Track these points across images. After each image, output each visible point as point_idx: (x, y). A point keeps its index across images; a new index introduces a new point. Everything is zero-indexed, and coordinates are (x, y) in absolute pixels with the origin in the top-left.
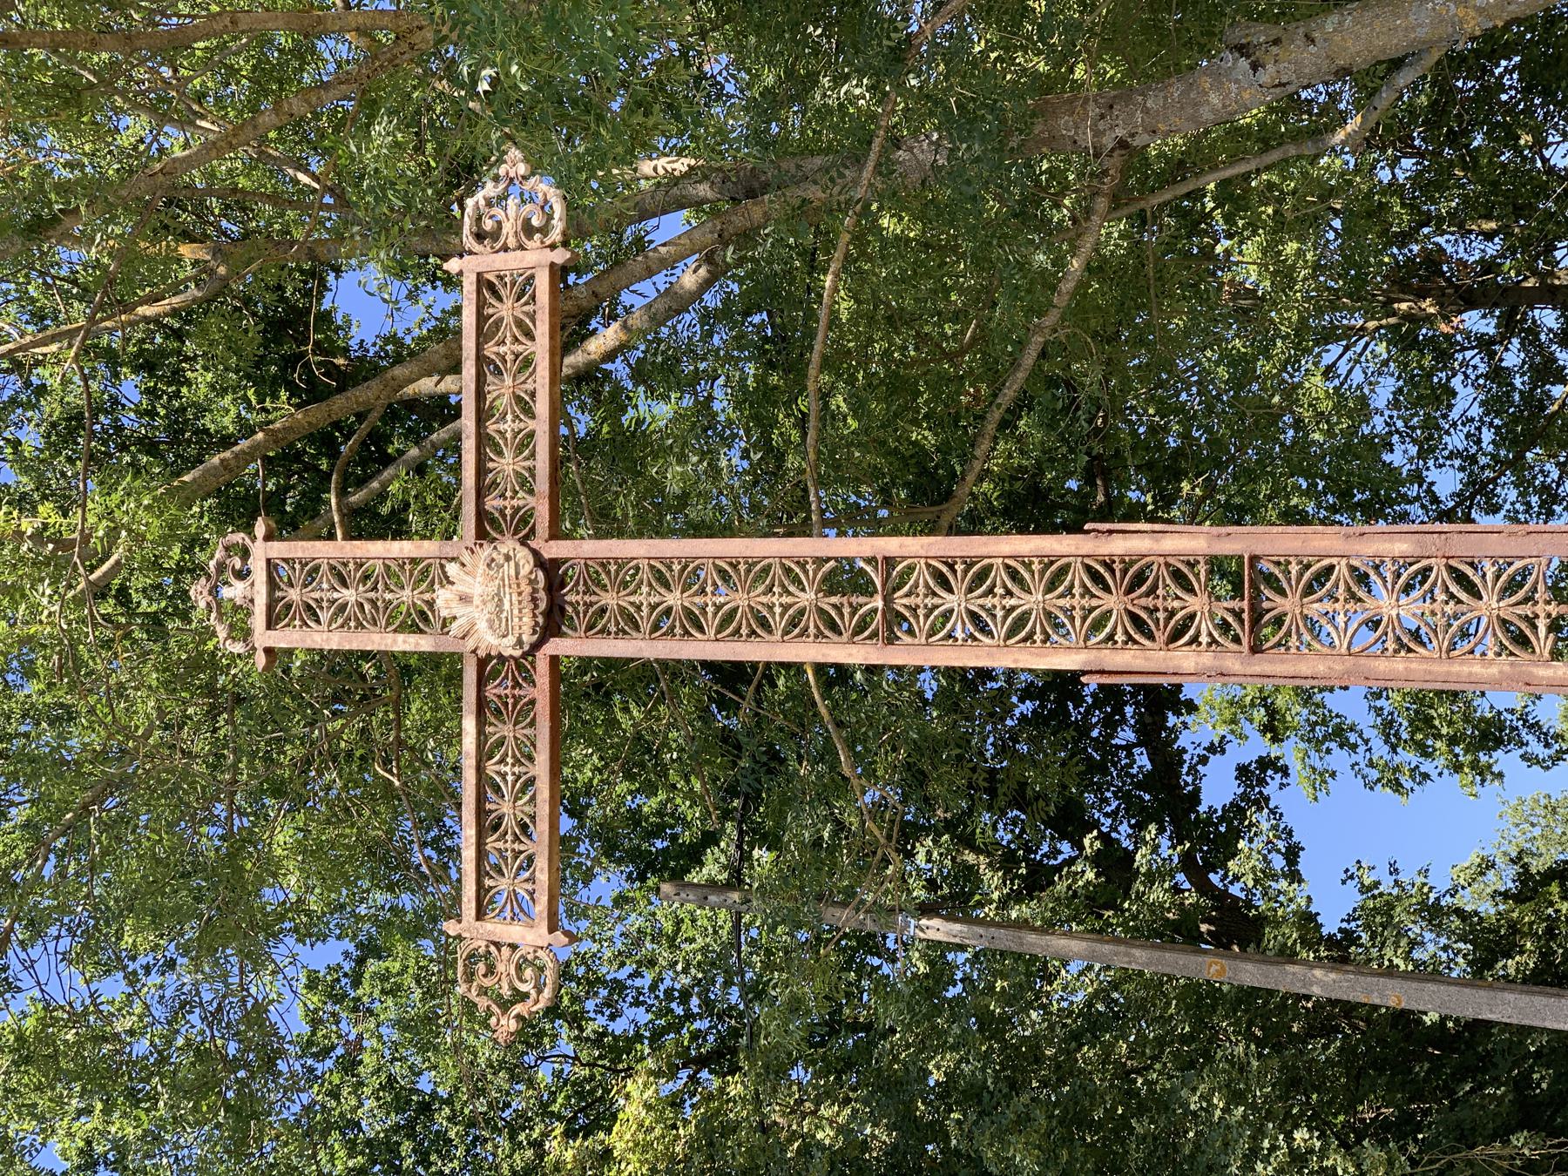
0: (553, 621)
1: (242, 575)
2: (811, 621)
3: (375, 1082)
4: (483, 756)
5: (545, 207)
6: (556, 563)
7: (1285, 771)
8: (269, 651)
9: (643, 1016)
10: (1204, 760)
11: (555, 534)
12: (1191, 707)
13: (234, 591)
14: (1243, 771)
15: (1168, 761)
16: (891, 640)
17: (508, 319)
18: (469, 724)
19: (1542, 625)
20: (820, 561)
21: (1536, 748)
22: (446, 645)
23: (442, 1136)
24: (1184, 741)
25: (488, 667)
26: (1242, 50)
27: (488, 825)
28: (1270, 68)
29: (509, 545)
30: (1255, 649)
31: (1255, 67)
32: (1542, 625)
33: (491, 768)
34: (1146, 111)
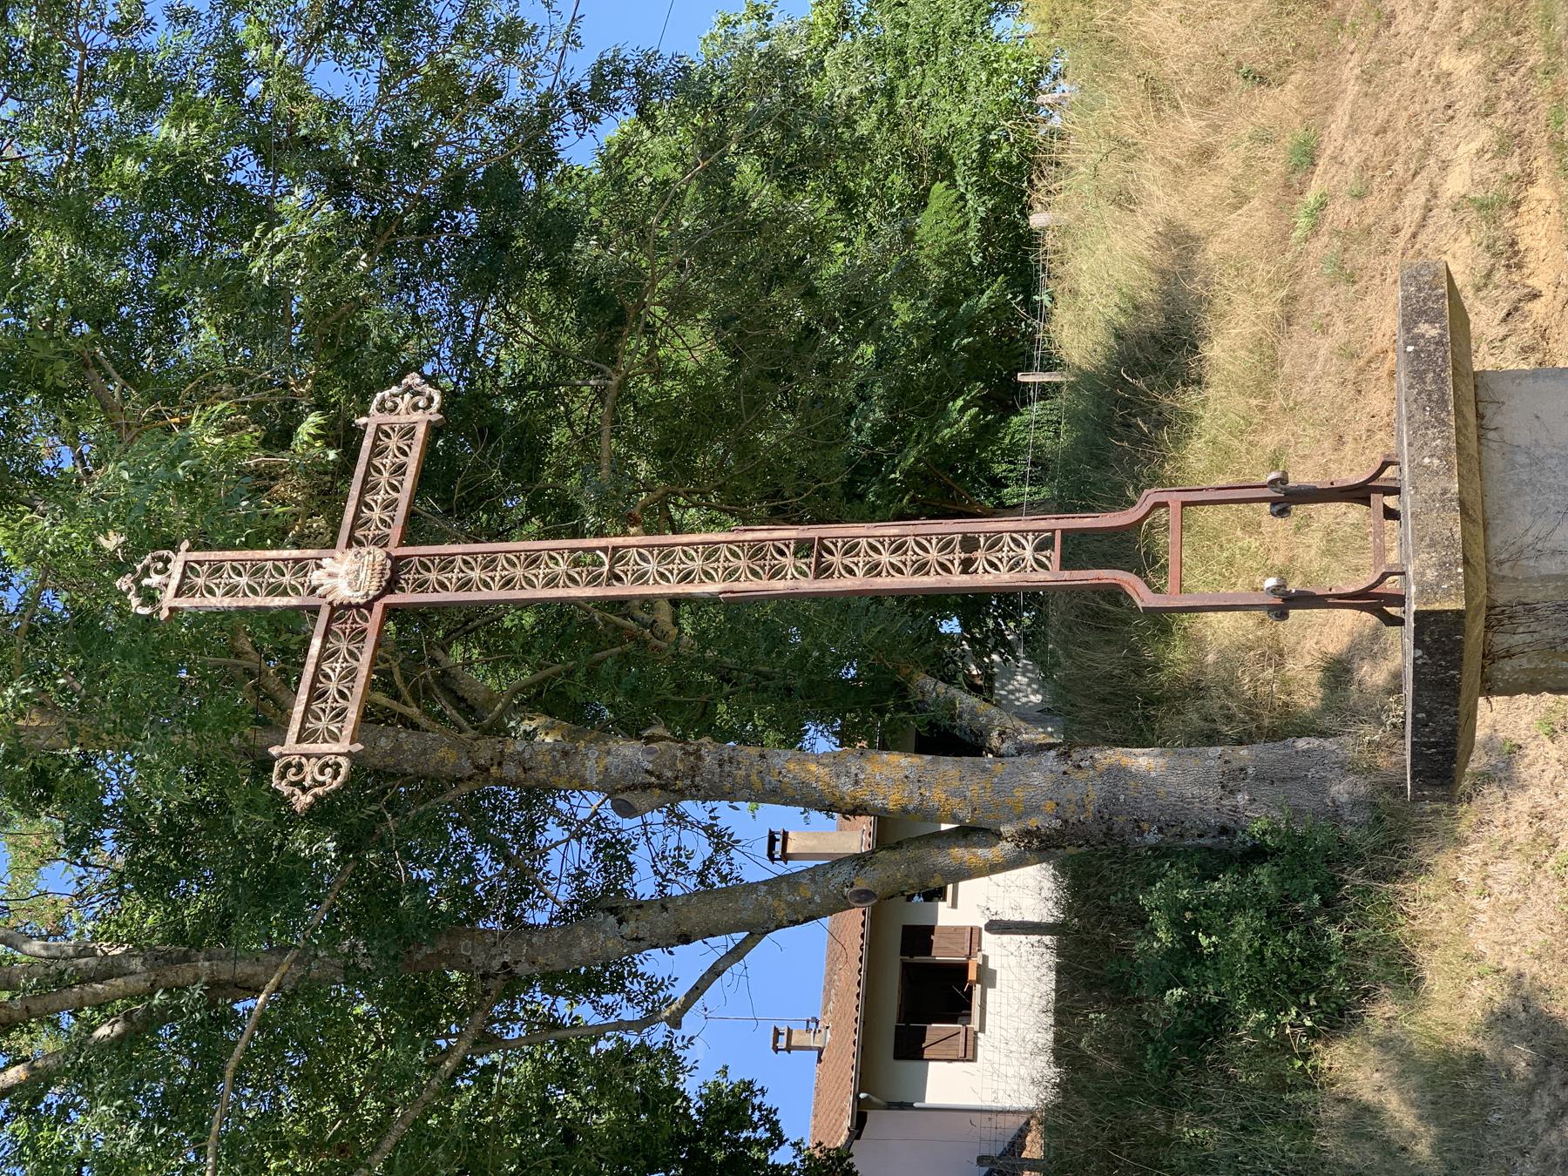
4: (321, 658)
13: (154, 580)
19: (956, 562)
22: (313, 601)
25: (340, 611)
27: (316, 694)
28: (632, 924)
31: (620, 922)
32: (956, 562)
34: (531, 945)
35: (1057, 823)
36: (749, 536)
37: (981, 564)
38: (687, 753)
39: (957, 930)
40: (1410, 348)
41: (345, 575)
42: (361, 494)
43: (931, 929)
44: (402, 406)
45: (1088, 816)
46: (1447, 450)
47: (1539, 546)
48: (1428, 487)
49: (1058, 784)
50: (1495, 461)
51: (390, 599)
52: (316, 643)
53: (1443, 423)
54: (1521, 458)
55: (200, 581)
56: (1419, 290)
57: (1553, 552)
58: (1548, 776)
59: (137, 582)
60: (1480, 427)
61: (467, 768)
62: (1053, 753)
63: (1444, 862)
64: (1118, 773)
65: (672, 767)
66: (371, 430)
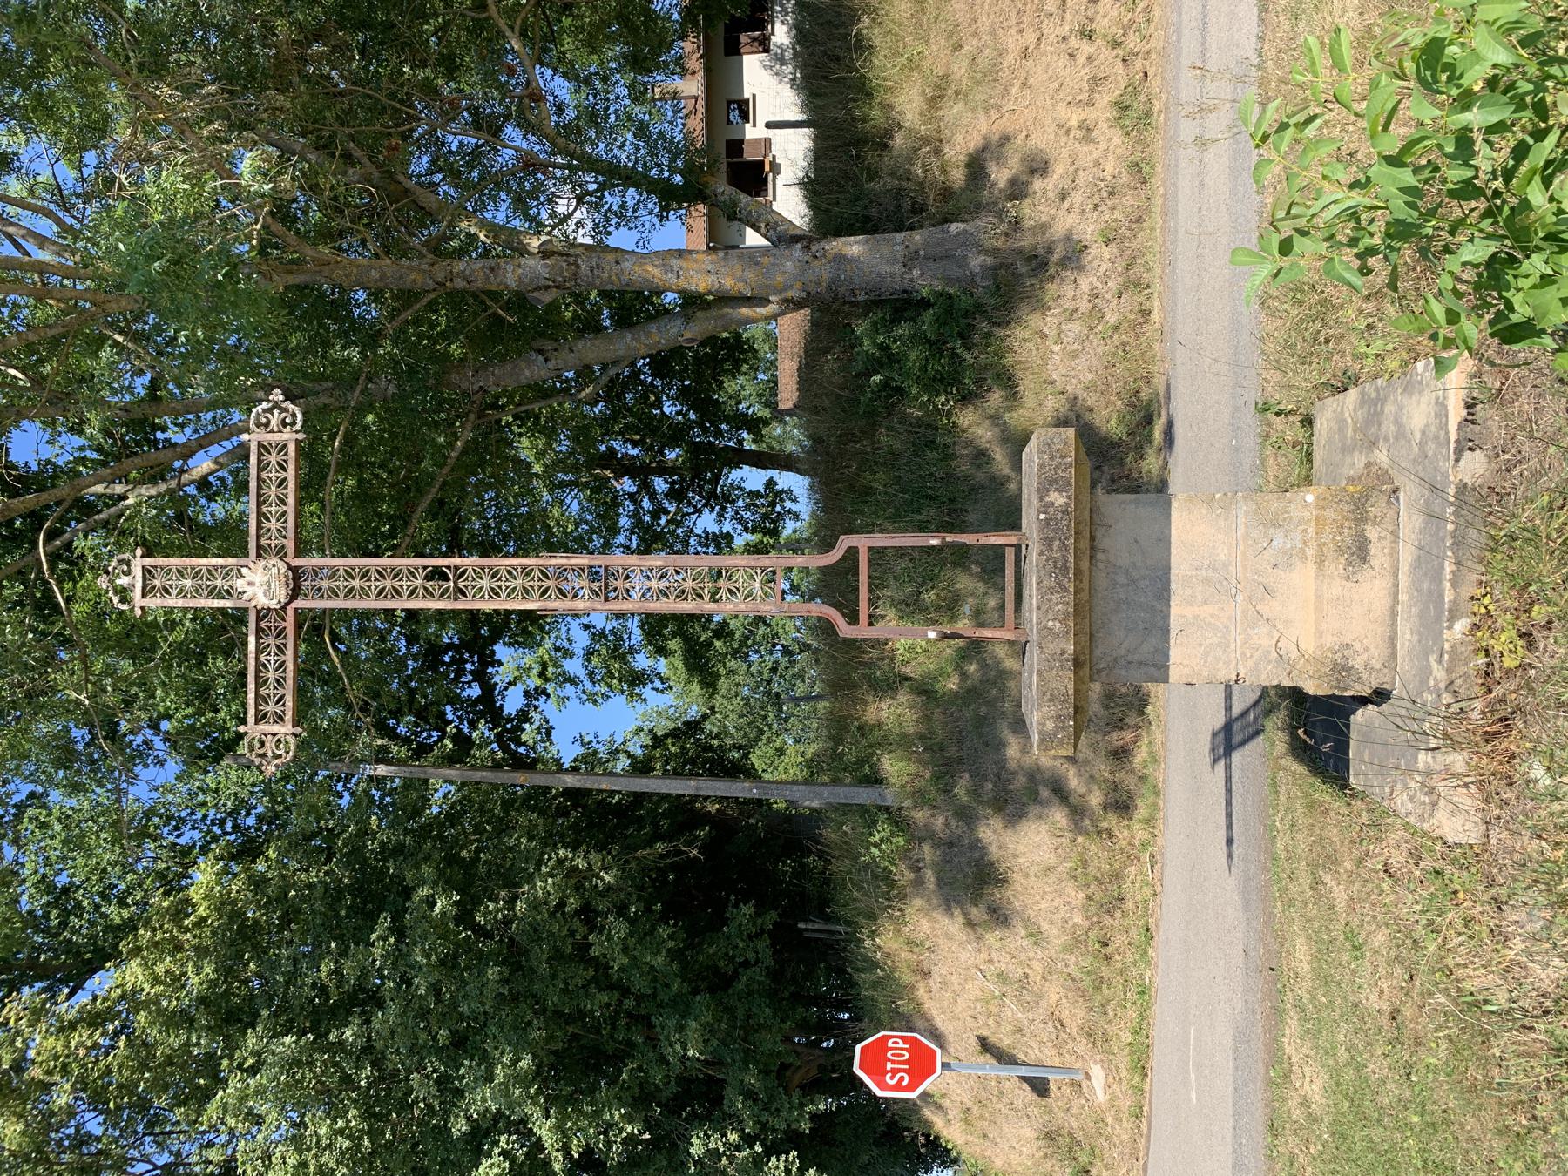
0: (294, 595)
1: (127, 573)
2: (420, 592)
3: (34, 879)
4: (258, 653)
5: (294, 415)
6: (297, 568)
7: (548, 696)
8: (142, 608)
9: (196, 835)
10: (506, 689)
11: (297, 555)
12: (500, 663)
13: (124, 581)
14: (527, 693)
15: (488, 688)
16: (456, 599)
17: (273, 462)
18: (252, 640)
20: (425, 568)
21: (658, 684)
23: (79, 905)
24: (497, 679)
25: (262, 614)
26: (540, 352)
27: (260, 682)
29: (275, 560)
30: (607, 600)
31: (546, 360)
33: (262, 657)
35: (803, 294)
36: (553, 562)
37: (723, 593)
38: (569, 264)
39: (757, 141)
40: (1042, 516)
41: (259, 584)
42: (258, 507)
43: (742, 141)
44: (274, 423)
45: (823, 289)
46: (1067, 614)
47: (1129, 658)
48: (1052, 647)
49: (803, 272)
50: (1102, 581)
51: (300, 603)
52: (252, 640)
53: (1065, 589)
54: (1121, 579)
55: (157, 582)
56: (1052, 458)
57: (1140, 663)
58: (1102, 270)
59: (111, 582)
60: (1092, 548)
61: (432, 285)
62: (799, 246)
63: (1034, 320)
64: (841, 259)
65: (561, 274)
66: (253, 447)
